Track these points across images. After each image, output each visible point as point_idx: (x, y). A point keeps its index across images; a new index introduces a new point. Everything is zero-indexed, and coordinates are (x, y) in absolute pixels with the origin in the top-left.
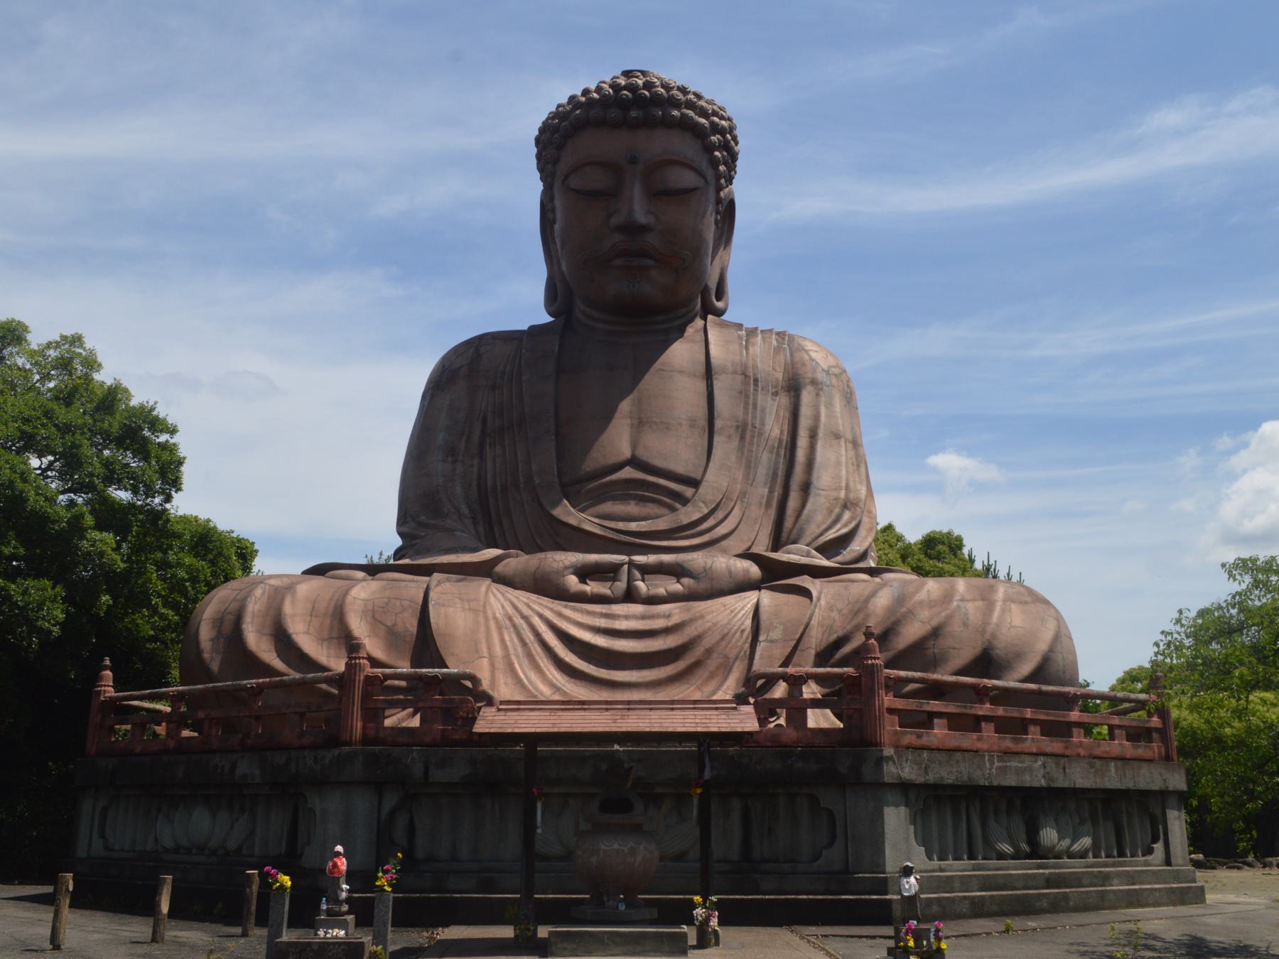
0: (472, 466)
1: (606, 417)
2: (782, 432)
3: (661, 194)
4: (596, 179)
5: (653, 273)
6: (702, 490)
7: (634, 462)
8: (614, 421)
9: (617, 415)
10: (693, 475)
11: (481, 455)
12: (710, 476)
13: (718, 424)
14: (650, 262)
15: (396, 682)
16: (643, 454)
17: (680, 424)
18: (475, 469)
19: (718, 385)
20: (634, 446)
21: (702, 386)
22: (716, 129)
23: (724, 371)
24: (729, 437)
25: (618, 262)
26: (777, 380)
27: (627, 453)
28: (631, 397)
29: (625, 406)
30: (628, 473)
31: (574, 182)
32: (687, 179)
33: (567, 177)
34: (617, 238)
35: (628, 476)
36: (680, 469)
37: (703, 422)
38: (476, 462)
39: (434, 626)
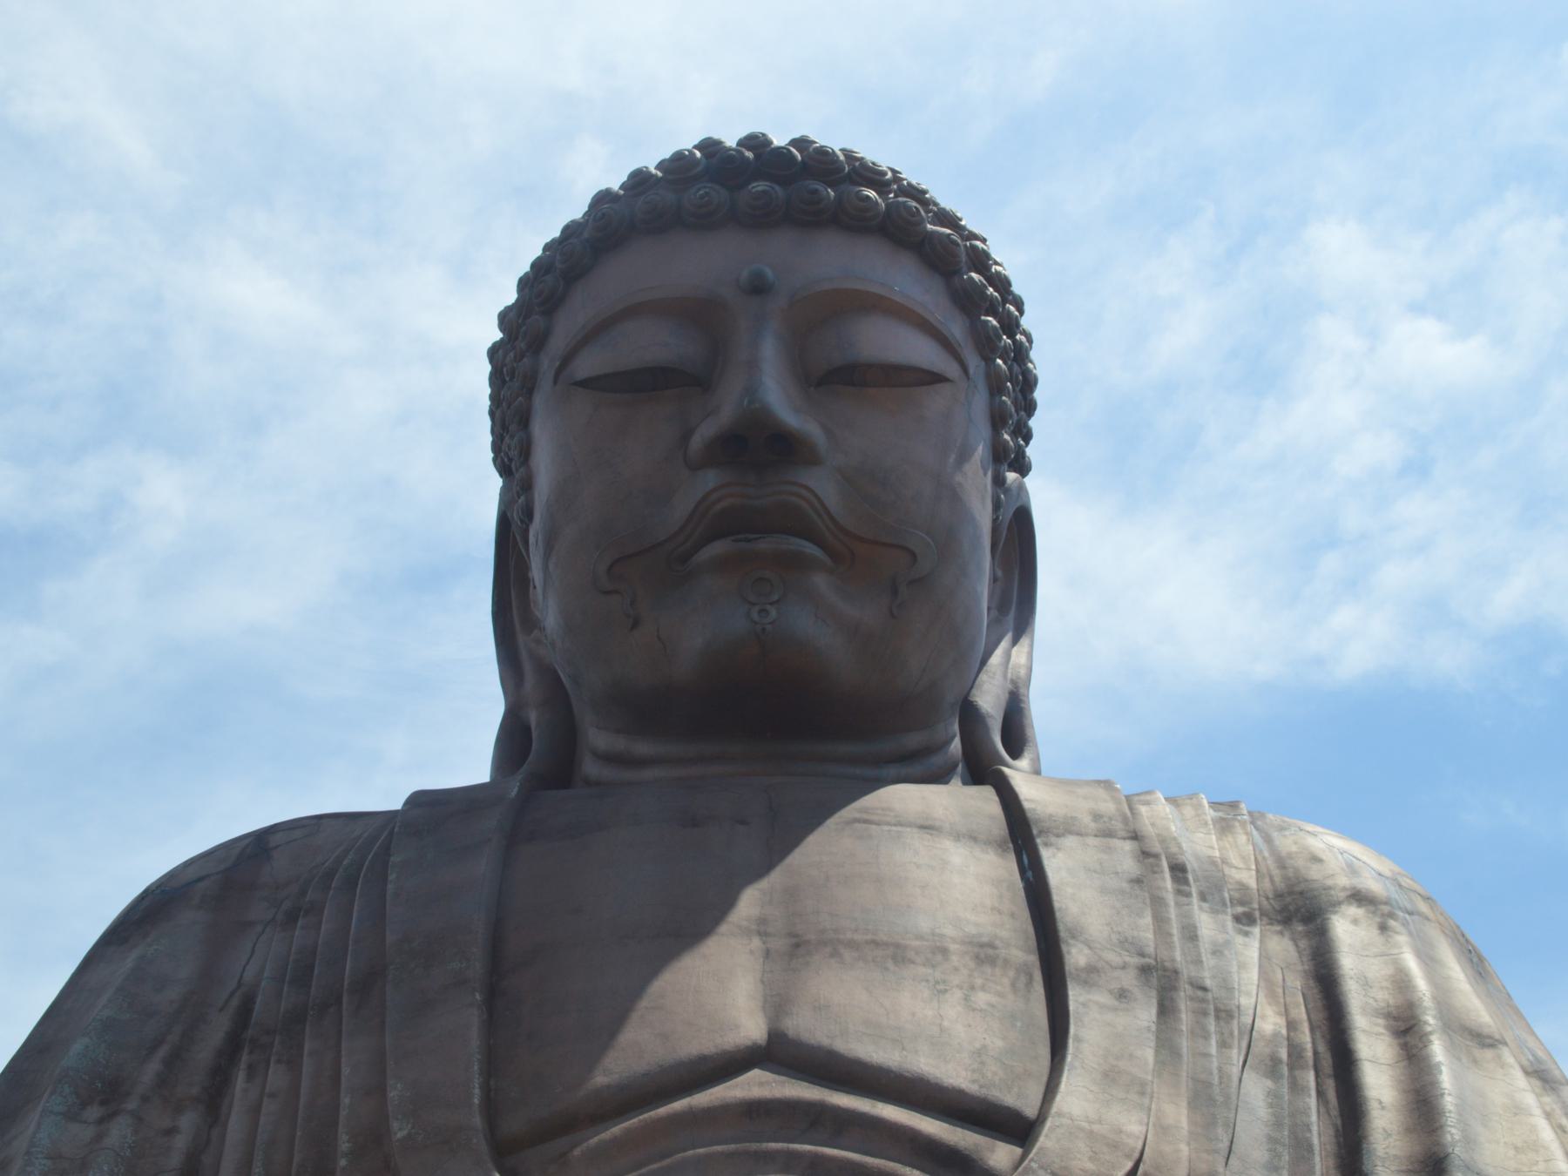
0: (170, 1132)
1: (690, 924)
2: (1291, 1025)
3: (842, 380)
4: (650, 344)
5: (821, 582)
6: (1046, 1140)
7: (779, 1053)
8: (711, 946)
9: (723, 928)
10: (1009, 1099)
11: (214, 1101)
12: (1076, 1098)
13: (1076, 956)
14: (811, 549)
15: (1026, 861)
16: (806, 1026)
17: (944, 951)
18: (181, 1143)
19: (1057, 863)
20: (777, 1004)
21: (1007, 867)
23: (1069, 828)
24: (1122, 995)
25: (718, 548)
26: (1243, 887)
27: (751, 1028)
28: (764, 884)
29: (750, 903)
30: (757, 1085)
31: (589, 364)
32: (917, 350)
33: (567, 360)
35: (757, 1093)
36: (954, 1074)
37: (1021, 950)
38: (188, 1122)
39: (1026, 805)
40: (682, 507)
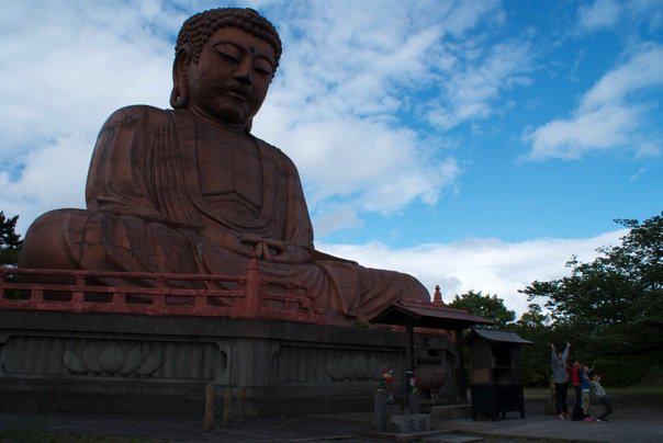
4: (231, 51)
22: (237, 17)
25: (233, 94)
31: (221, 48)
34: (236, 83)
40: (229, 83)
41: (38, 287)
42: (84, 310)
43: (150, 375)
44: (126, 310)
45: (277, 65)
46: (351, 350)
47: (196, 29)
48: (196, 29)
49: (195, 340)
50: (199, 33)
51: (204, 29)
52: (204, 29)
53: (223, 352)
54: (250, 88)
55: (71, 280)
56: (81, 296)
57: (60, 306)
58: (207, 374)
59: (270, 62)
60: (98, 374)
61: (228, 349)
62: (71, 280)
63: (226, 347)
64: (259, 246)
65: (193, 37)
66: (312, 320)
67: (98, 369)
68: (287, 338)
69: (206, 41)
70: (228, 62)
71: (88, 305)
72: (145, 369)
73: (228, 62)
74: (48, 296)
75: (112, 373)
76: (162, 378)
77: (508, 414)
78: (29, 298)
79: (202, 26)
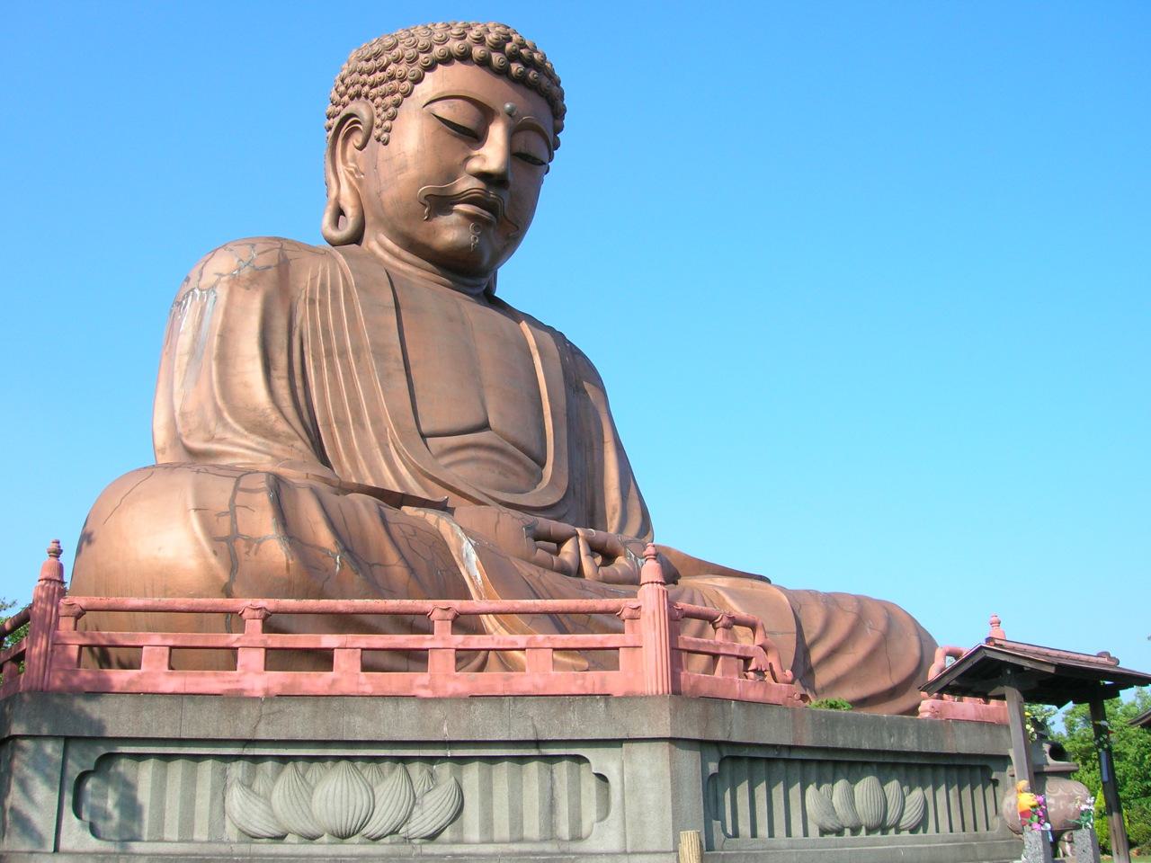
41: (156, 639)
42: (267, 691)
43: (432, 838)
44: (368, 689)
45: (557, 145)
46: (851, 764)
47: (383, 69)
48: (383, 69)
49: (536, 751)
50: (392, 77)
51: (402, 68)
52: (402, 68)
53: (602, 778)
54: (506, 195)
55: (233, 620)
56: (257, 657)
57: (211, 682)
58: (564, 830)
59: (547, 142)
60: (312, 838)
61: (612, 772)
62: (233, 620)
63: (599, 760)
64: (568, 547)
65: (373, 86)
66: (773, 698)
67: (311, 829)
68: (736, 738)
69: (407, 94)
70: (1142, 680)
71: (278, 680)
72: (423, 823)
73: (1142, 680)
74: (177, 658)
75: (344, 836)
76: (460, 842)
77: (1051, 670)
78: (139, 668)
79: (397, 61)
